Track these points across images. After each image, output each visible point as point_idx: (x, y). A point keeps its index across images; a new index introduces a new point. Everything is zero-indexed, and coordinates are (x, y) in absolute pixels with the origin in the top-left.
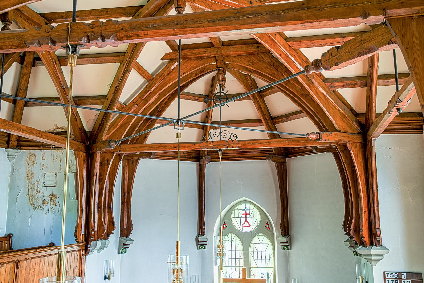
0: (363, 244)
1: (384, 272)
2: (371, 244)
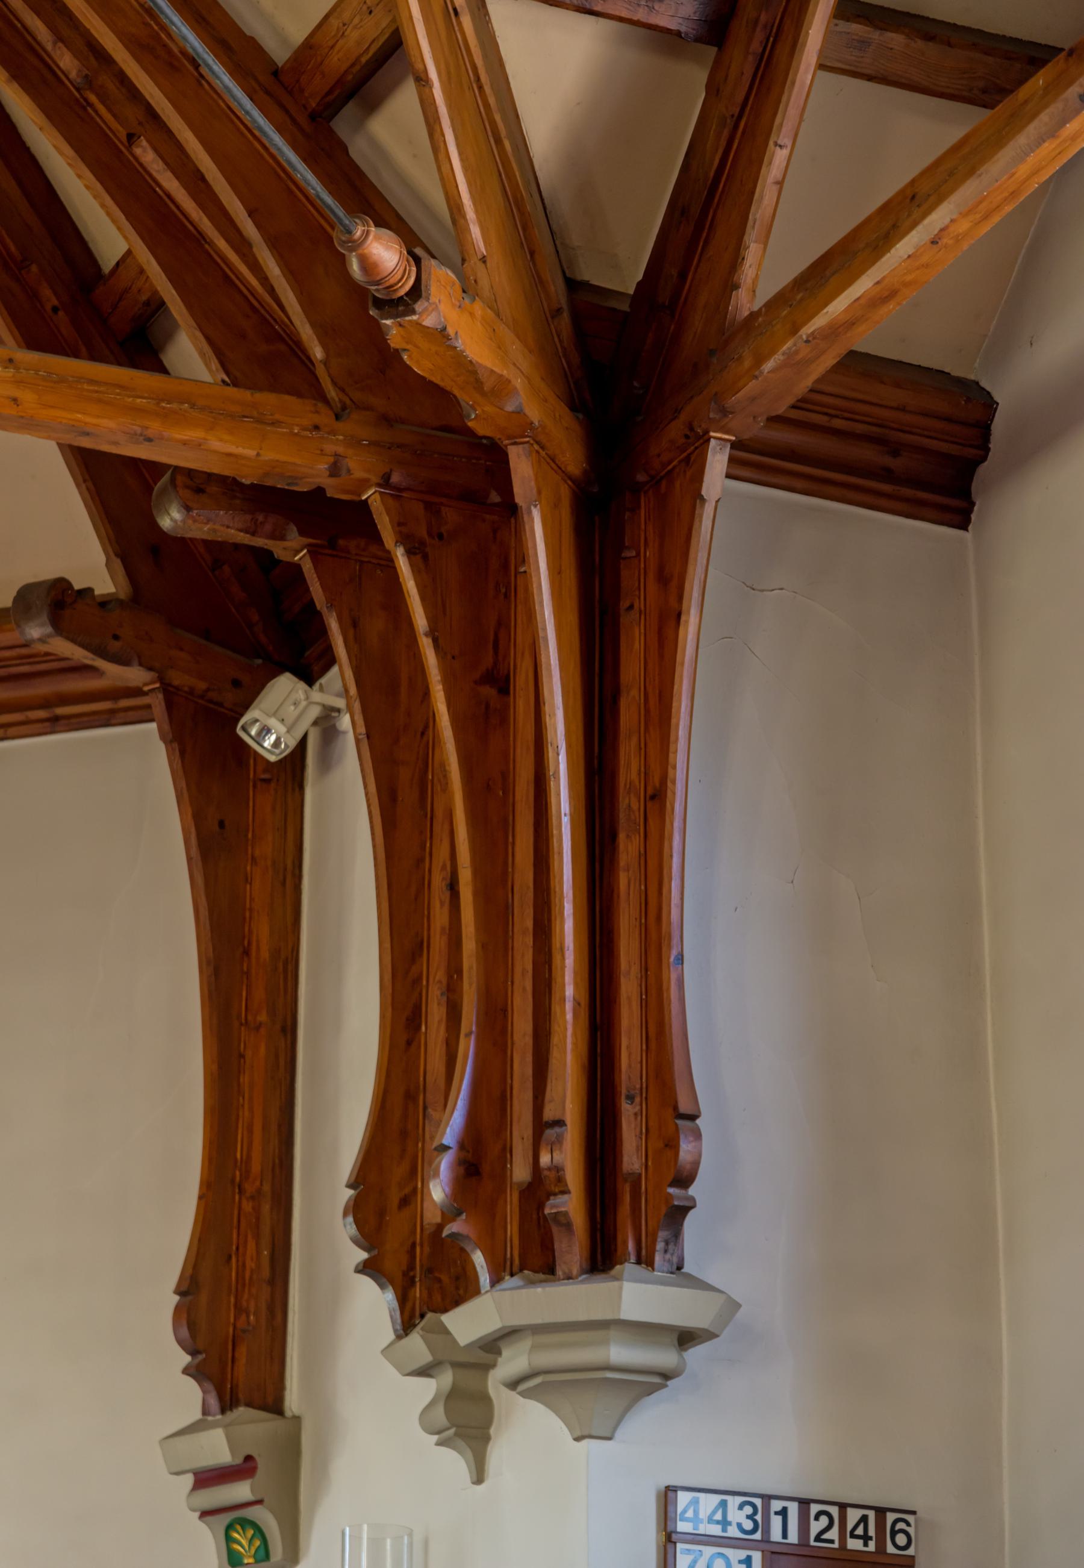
0: (538, 1260)
1: (667, 1496)
2: (602, 1259)
